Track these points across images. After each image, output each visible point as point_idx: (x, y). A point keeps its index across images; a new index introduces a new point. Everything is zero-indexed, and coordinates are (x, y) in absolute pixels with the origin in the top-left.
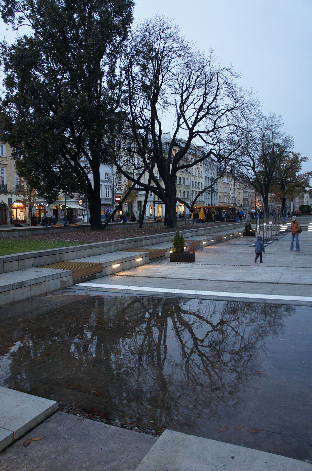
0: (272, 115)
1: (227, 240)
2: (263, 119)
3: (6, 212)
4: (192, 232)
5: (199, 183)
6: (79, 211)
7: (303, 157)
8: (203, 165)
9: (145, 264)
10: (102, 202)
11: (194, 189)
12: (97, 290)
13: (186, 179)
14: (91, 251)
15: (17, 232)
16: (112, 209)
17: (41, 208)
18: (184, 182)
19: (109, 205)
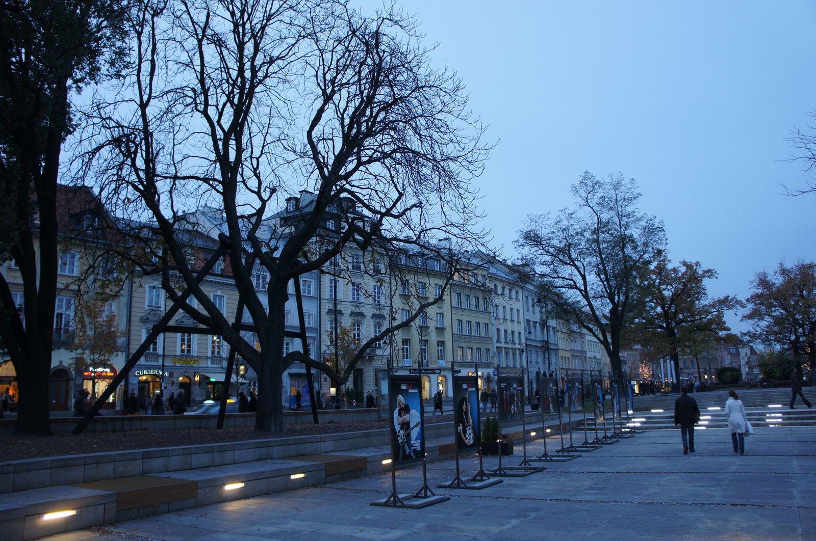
3: (67, 385)
5: (513, 332)
7: (706, 269)
8: (520, 297)
10: (673, 420)
11: (503, 345)
13: (482, 326)
18: (479, 331)
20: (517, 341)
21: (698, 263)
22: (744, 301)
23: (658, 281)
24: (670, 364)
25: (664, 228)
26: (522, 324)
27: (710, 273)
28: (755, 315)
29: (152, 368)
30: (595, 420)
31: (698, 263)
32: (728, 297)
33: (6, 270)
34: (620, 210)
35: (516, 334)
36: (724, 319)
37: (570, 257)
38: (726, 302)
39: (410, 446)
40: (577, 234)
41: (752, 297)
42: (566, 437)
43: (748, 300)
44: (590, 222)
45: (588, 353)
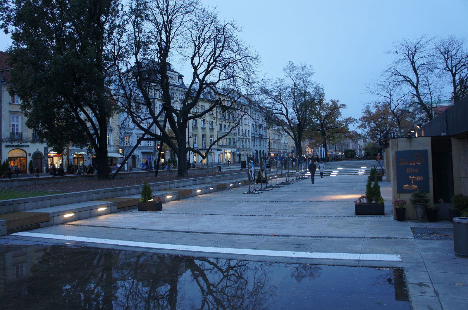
0: (303, 65)
1: (232, 188)
2: (294, 68)
3: (41, 161)
4: (194, 180)
5: (246, 130)
6: (119, 159)
9: (111, 213)
12: (21, 239)
14: (55, 201)
15: (16, 182)
16: (154, 157)
17: (80, 157)
19: (151, 153)
20: (247, 135)
21: (338, 100)
22: (358, 120)
23: (319, 109)
24: (323, 149)
25: (323, 89)
26: (250, 126)
27: (343, 106)
28: (362, 126)
29: (78, 151)
30: (296, 172)
31: (338, 100)
32: (351, 117)
33: (8, 104)
34: (304, 79)
35: (247, 131)
36: (348, 128)
37: (280, 99)
38: (350, 120)
39: (252, 177)
40: (284, 89)
41: (362, 118)
42: (288, 178)
43: (359, 119)
44: (290, 84)
45: (281, 140)
